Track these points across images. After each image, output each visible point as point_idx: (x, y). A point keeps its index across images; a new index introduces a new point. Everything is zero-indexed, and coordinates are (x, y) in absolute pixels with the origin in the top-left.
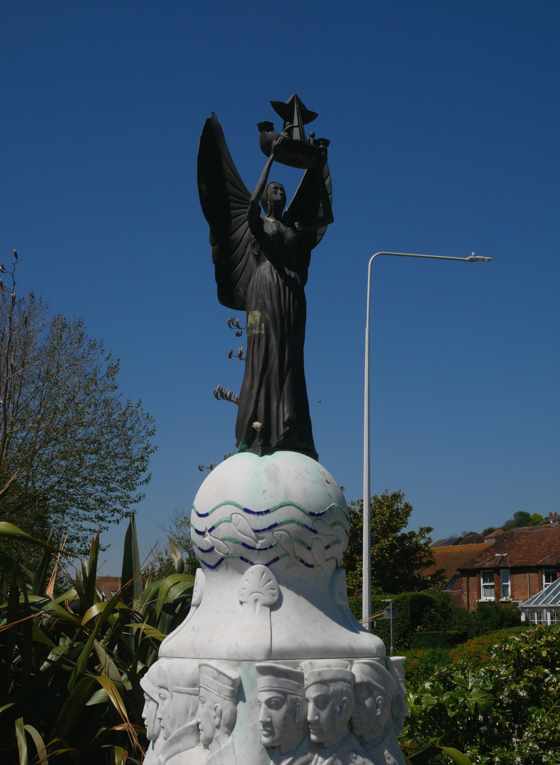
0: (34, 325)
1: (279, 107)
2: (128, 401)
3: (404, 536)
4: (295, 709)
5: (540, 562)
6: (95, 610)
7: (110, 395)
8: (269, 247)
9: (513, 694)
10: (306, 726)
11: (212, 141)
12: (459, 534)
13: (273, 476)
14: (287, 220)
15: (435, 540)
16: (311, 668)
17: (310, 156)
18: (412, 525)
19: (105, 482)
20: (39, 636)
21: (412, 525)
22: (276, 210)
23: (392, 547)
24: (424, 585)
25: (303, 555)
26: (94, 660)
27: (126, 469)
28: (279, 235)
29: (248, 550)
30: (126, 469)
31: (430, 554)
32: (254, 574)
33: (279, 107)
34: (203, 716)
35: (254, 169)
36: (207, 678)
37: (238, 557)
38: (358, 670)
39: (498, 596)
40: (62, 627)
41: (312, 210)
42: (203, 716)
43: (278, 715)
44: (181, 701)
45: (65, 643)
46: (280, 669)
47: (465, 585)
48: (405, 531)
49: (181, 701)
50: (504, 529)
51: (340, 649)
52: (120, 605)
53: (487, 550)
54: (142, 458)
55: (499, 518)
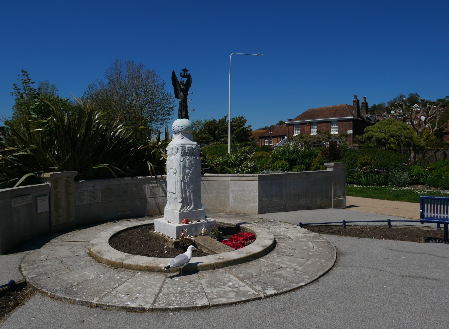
0: (142, 71)
1: (183, 70)
3: (244, 128)
4: (185, 151)
6: (160, 143)
7: (162, 91)
8: (182, 90)
9: (241, 158)
10: (186, 153)
12: (263, 127)
14: (184, 86)
16: (187, 146)
17: (189, 77)
18: (246, 125)
20: (150, 148)
21: (246, 125)
22: (183, 85)
23: (241, 131)
24: (249, 141)
25: (185, 132)
26: (160, 153)
27: (168, 111)
28: (183, 88)
30: (168, 111)
32: (180, 134)
33: (183, 70)
34: (174, 152)
35: (179, 78)
36: (174, 147)
38: (193, 146)
39: (269, 144)
40: (153, 147)
41: (188, 84)
42: (174, 152)
43: (183, 151)
44: (171, 150)
45: (155, 150)
46: (183, 146)
48: (244, 127)
49: (171, 150)
51: (191, 144)
52: (164, 142)
55: (274, 123)
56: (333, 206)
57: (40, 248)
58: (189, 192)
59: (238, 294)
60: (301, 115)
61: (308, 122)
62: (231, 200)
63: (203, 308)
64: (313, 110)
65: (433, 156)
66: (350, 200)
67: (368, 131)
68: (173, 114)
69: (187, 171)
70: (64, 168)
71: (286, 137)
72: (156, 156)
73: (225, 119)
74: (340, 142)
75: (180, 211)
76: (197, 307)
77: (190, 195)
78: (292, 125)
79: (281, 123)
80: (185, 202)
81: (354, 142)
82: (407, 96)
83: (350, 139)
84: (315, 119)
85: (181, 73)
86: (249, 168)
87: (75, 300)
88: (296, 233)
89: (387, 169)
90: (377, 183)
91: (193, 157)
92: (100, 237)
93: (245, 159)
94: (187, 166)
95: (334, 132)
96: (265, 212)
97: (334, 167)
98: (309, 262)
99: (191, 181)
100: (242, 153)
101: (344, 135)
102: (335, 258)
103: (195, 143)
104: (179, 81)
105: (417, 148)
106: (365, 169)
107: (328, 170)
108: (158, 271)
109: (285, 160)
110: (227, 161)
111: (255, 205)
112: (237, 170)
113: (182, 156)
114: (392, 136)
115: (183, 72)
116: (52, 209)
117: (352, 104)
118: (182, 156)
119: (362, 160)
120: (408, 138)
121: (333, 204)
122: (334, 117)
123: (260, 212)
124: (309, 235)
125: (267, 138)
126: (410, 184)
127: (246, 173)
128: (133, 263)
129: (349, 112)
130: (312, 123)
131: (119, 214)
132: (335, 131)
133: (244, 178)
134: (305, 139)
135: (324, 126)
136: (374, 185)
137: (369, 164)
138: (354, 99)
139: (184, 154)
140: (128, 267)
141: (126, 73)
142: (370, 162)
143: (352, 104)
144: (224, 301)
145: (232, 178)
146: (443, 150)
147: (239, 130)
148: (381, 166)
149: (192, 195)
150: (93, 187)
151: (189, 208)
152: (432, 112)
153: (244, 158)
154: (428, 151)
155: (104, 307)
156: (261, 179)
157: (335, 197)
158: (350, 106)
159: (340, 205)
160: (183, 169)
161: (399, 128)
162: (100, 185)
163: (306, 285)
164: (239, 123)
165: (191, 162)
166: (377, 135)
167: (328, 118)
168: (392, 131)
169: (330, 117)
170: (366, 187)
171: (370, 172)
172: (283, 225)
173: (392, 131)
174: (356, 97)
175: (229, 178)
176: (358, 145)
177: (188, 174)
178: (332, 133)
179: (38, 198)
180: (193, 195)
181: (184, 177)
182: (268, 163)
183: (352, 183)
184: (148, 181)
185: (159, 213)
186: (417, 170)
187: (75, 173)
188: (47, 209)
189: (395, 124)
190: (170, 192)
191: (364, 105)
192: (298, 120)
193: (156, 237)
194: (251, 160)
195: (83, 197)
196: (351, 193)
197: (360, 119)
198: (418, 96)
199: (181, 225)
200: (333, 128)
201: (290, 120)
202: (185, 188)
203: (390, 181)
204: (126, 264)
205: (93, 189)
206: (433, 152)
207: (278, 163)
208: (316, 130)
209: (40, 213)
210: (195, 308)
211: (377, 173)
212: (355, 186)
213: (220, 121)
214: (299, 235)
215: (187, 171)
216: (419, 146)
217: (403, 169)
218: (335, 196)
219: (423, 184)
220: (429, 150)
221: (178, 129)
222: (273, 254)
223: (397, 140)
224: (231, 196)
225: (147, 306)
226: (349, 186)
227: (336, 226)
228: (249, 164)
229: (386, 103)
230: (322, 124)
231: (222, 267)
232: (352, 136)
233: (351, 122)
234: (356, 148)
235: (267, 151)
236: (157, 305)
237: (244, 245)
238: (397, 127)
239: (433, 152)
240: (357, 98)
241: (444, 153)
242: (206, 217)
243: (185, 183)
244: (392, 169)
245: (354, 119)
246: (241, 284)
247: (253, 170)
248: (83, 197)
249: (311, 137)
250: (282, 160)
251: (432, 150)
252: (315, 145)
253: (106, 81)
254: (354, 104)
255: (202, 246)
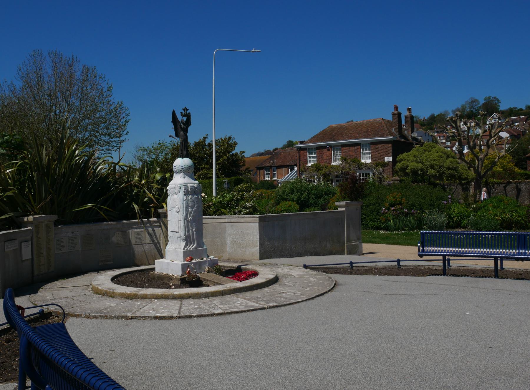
1: (183, 109)
2: (118, 102)
3: (233, 154)
4: (187, 190)
5: (288, 164)
8: (183, 129)
9: (237, 198)
11: (174, 113)
12: (262, 151)
13: (184, 161)
15: (246, 156)
17: (188, 116)
18: (237, 150)
19: (109, 135)
21: (237, 150)
22: (183, 124)
23: (228, 158)
24: (241, 174)
29: (334, 290)
31: (244, 161)
32: (182, 174)
33: (183, 109)
35: (180, 118)
37: (180, 172)
38: (195, 185)
39: (271, 178)
41: (188, 123)
46: (185, 185)
47: (258, 173)
48: (233, 152)
50: (282, 148)
51: (193, 183)
53: (268, 159)
54: (125, 125)
55: (278, 143)
56: (346, 252)
57: (37, 293)
58: (192, 230)
59: (246, 306)
60: (317, 135)
61: (328, 145)
62: (229, 245)
63: (220, 314)
64: (335, 128)
65: (502, 191)
66: (366, 247)
67: (402, 160)
68: (126, 134)
69: (190, 210)
70: (42, 211)
71: (296, 168)
72: (141, 197)
73: (205, 141)
74: (374, 174)
75: (184, 249)
76: (214, 314)
77: (193, 234)
78: (305, 149)
79: (290, 144)
80: (188, 240)
81: (394, 173)
82: (482, 102)
83: (389, 169)
84: (339, 140)
85: (181, 113)
86: (248, 209)
87: (111, 316)
88: (298, 272)
89: (421, 209)
90: (409, 227)
91: (196, 196)
92: (103, 280)
93: (243, 198)
94: (190, 205)
95: (366, 159)
96: (267, 258)
97: (347, 206)
98: (308, 289)
99: (194, 220)
100: (239, 191)
101: (380, 163)
102: (332, 286)
103: (197, 182)
104: (180, 121)
105: (463, 182)
106: (393, 210)
107: (339, 209)
108: (173, 298)
109: (293, 200)
110: (220, 202)
111: (256, 250)
112: (234, 212)
113: (185, 195)
114: (432, 167)
115: (183, 111)
116: (35, 256)
117: (390, 118)
118: (185, 195)
119: (390, 198)
120: (451, 169)
121: (346, 250)
122: (364, 138)
123: (261, 258)
124: (312, 273)
125: (268, 169)
126: (449, 227)
127: (243, 214)
128: (148, 293)
129: (386, 130)
130: (333, 146)
131: (100, 264)
132: (367, 158)
133: (242, 220)
134: (324, 170)
135: (351, 151)
136: (405, 230)
137: (398, 204)
138: (393, 110)
139: (186, 193)
140: (144, 297)
141: (50, 72)
142: (400, 202)
143: (390, 118)
144: (235, 310)
145: (229, 220)
146: (515, 183)
147: (225, 157)
148: (413, 205)
149: (194, 234)
150: (73, 233)
151: (193, 247)
152: (495, 132)
153: (241, 197)
154: (495, 186)
155: (139, 318)
156: (261, 220)
157: (348, 241)
158: (388, 121)
159: (354, 251)
160: (186, 208)
161: (441, 156)
162: (78, 231)
163: (303, 301)
164: (226, 146)
165: (194, 201)
166: (412, 165)
167: (357, 138)
168: (432, 160)
169: (360, 138)
170: (394, 232)
171: (400, 213)
172: (286, 267)
173: (432, 160)
174: (396, 108)
175: (226, 220)
176: (398, 178)
177: (191, 213)
178: (363, 161)
179: (23, 244)
180: (196, 234)
181: (187, 215)
182: (270, 205)
183: (378, 228)
184: (132, 226)
185: (147, 263)
186: (456, 209)
187: (55, 217)
188: (31, 257)
189: (436, 150)
190: (172, 232)
191: (409, 119)
192: (314, 142)
193: (158, 277)
194: (250, 199)
195: (62, 244)
196: (374, 240)
197: (402, 140)
198: (498, 100)
199: (186, 262)
200: (364, 154)
201: (302, 143)
202: (188, 227)
203: (425, 225)
204: (141, 294)
205: (71, 235)
206: (502, 186)
207: (284, 205)
208: (339, 157)
209: (24, 260)
210: (213, 315)
211: (407, 215)
212: (382, 232)
213: (196, 144)
214: (301, 273)
215: (190, 210)
216: (466, 179)
217: (441, 209)
218: (348, 241)
219: (466, 228)
220: (496, 183)
221: (180, 168)
222: (276, 286)
223: (438, 172)
224: (228, 240)
225: (175, 315)
226: (375, 232)
227: (343, 267)
228: (248, 204)
229: (450, 112)
230: (348, 148)
231: (230, 294)
232: (391, 165)
233: (390, 145)
234: (396, 182)
235: (268, 189)
236: (182, 314)
237: (247, 279)
238: (437, 154)
239: (502, 186)
240: (397, 110)
241: (517, 187)
242: (208, 256)
243: (188, 221)
244: (427, 209)
245: (394, 141)
246: (248, 302)
247: (253, 211)
248: (62, 244)
249: (333, 167)
250: (289, 200)
251: (500, 183)
252: (339, 179)
253: (19, 84)
254: (393, 118)
255: (208, 280)
